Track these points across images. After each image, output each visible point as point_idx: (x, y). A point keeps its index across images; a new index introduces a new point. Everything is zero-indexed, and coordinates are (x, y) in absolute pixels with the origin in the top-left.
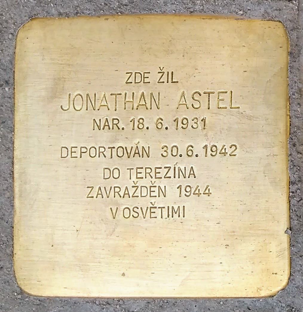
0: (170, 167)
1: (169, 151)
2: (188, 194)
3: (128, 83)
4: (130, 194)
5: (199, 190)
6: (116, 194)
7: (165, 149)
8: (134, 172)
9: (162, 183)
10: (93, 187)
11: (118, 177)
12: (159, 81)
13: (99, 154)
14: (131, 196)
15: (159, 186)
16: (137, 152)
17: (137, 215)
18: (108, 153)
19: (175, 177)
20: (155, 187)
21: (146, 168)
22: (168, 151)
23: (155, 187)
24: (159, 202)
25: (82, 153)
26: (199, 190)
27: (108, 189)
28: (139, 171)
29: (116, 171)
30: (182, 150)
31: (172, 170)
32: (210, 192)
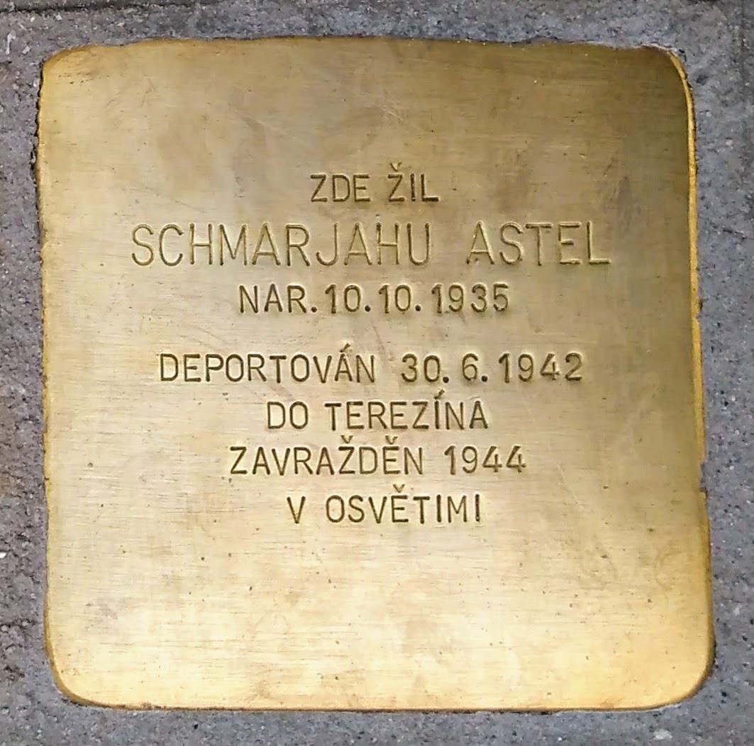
0: (425, 404)
1: (419, 367)
2: (470, 467)
3: (315, 200)
4: (333, 465)
5: (520, 456)
6: (301, 465)
7: (410, 361)
8: (341, 413)
9: (413, 441)
10: (244, 449)
11: (306, 423)
12: (316, 198)
13: (249, 372)
14: (336, 470)
15: (406, 449)
16: (343, 368)
17: (360, 513)
18: (269, 369)
19: (437, 427)
20: (396, 449)
21: (348, 404)
22: (417, 367)
23: (396, 449)
24: (413, 485)
25: (211, 371)
26: (520, 456)
27: (281, 455)
28: (353, 409)
29: (298, 411)
30: (450, 364)
31: (431, 408)
32: (523, 462)
